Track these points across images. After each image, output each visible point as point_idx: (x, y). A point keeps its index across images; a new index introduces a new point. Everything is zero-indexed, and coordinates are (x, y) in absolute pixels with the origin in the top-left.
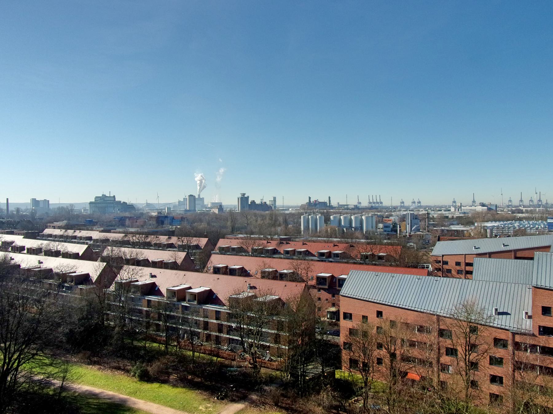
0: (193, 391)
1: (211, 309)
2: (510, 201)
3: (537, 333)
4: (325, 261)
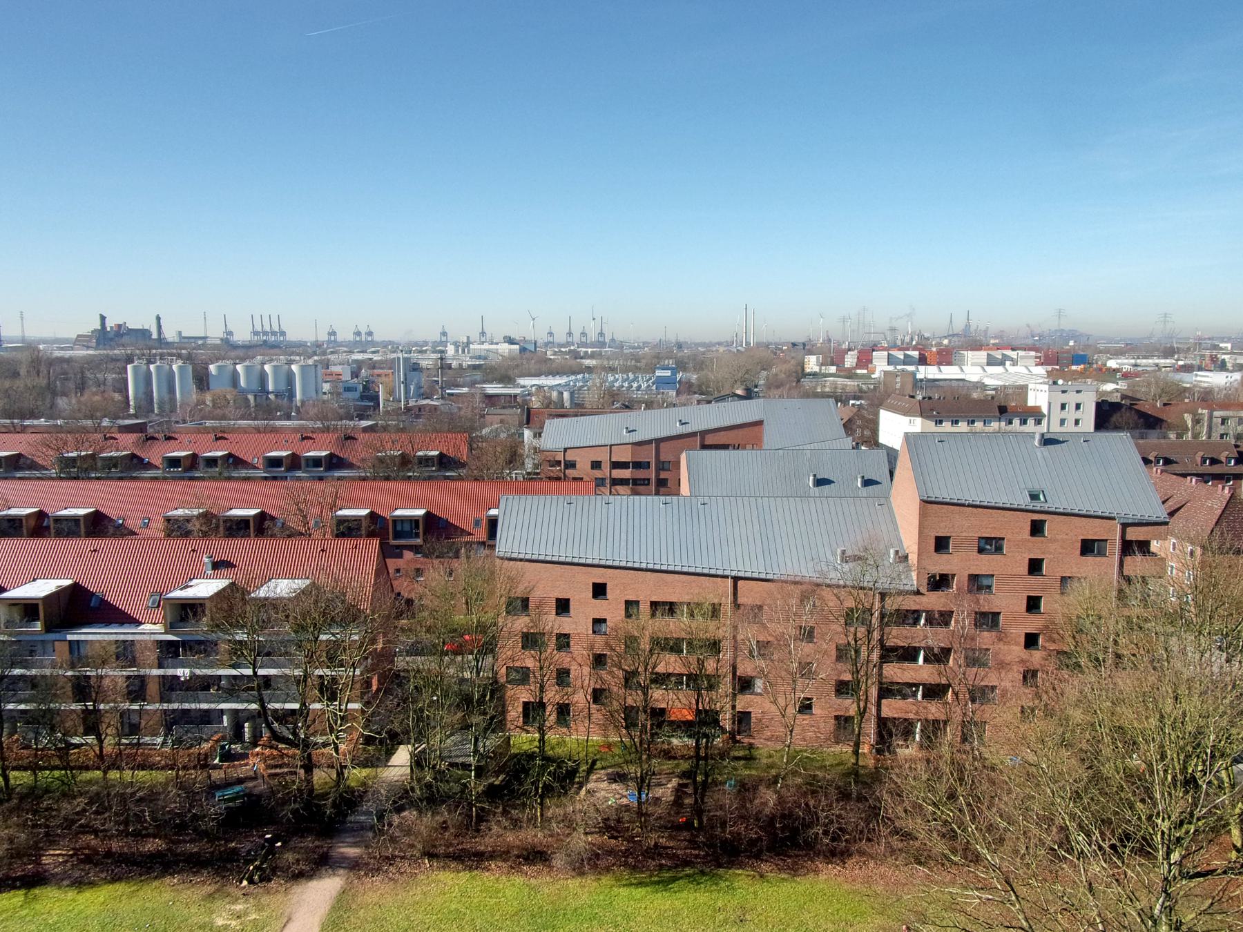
0: (156, 883)
1: (106, 638)
2: (551, 334)
3: (923, 590)
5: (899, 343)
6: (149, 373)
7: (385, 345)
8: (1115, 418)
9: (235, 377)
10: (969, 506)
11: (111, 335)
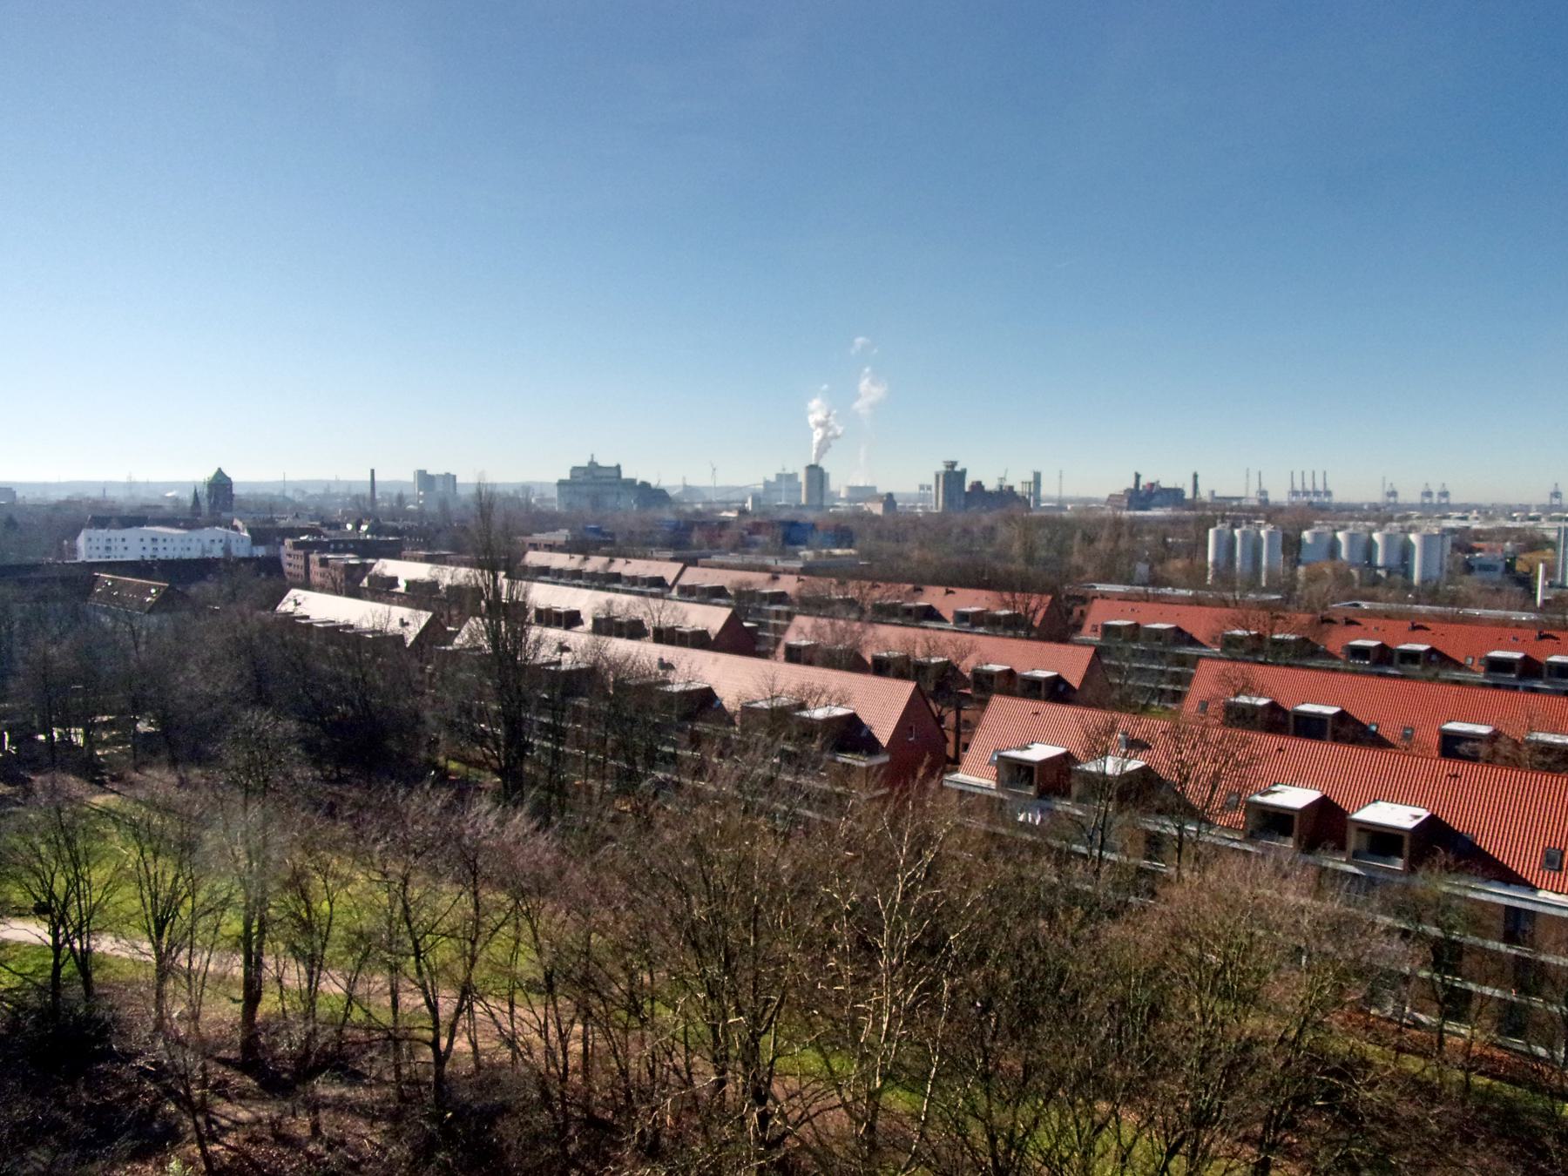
1: (1494, 899)
2: (1556, 494)
4: (1516, 688)
6: (1233, 538)
7: (1467, 509)
9: (1334, 547)
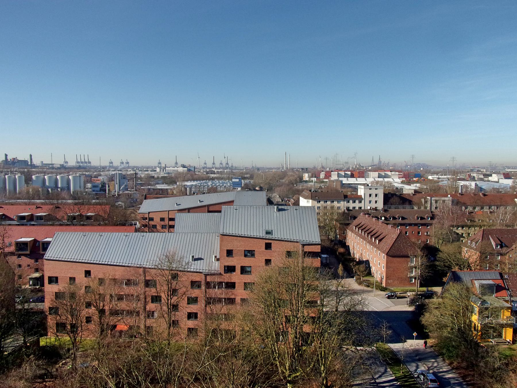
2: (205, 163)
3: (223, 272)
4: (26, 225)
5: (351, 169)
6: (5, 179)
8: (391, 200)
10: (240, 237)
11: (10, 163)
